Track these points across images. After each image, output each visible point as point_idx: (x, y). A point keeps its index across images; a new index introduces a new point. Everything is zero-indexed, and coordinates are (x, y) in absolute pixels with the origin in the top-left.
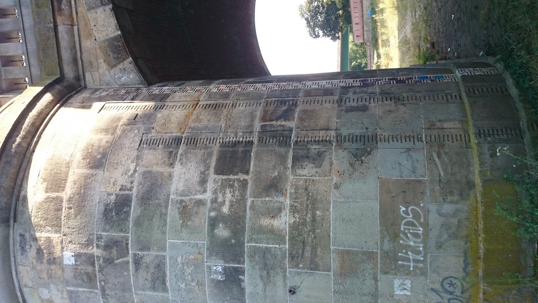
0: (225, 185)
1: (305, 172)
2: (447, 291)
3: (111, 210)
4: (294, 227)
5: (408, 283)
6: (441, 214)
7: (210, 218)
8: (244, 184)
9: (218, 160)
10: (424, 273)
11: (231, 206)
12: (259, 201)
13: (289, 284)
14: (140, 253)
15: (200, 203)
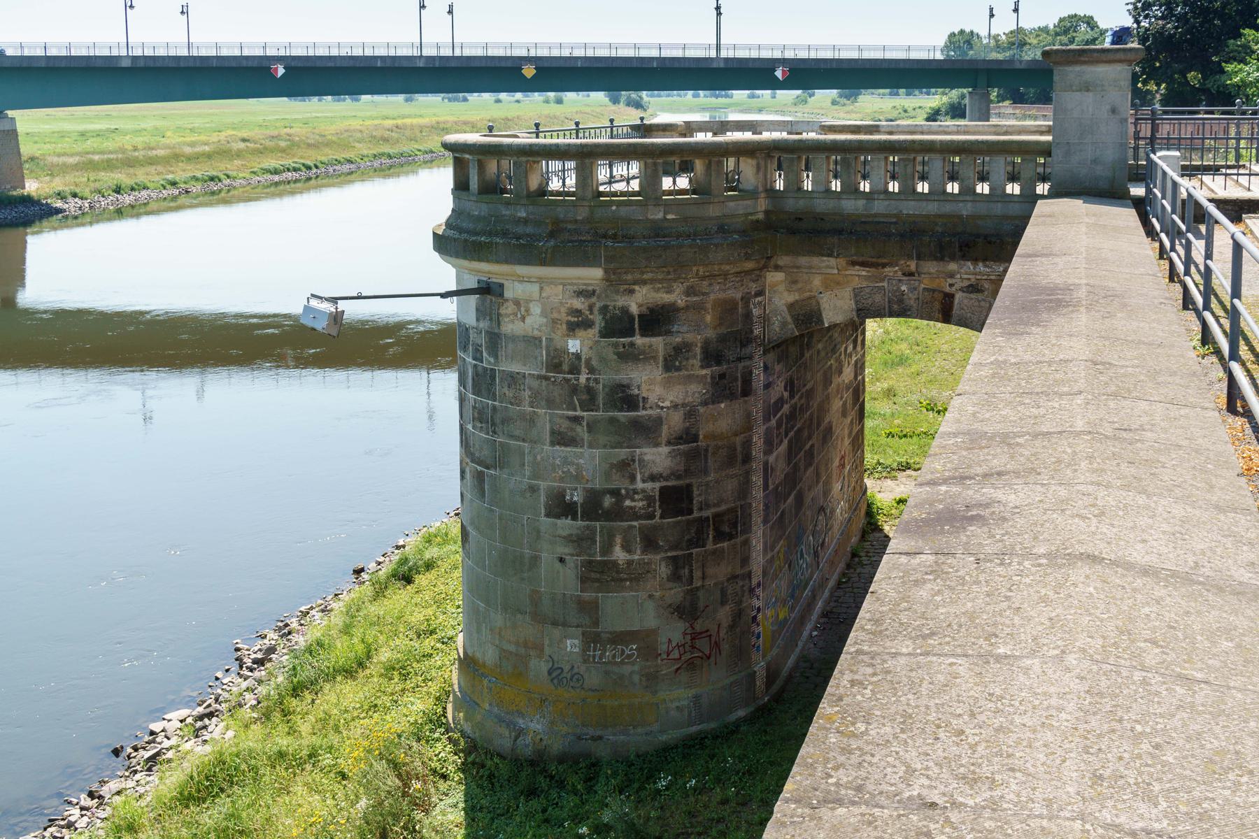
0: (649, 499)
1: (663, 569)
2: (572, 677)
3: (623, 392)
4: (615, 563)
5: (577, 650)
6: (632, 673)
7: (619, 490)
9: (674, 487)
10: (585, 661)
11: (631, 508)
14: (585, 424)
15: (633, 479)
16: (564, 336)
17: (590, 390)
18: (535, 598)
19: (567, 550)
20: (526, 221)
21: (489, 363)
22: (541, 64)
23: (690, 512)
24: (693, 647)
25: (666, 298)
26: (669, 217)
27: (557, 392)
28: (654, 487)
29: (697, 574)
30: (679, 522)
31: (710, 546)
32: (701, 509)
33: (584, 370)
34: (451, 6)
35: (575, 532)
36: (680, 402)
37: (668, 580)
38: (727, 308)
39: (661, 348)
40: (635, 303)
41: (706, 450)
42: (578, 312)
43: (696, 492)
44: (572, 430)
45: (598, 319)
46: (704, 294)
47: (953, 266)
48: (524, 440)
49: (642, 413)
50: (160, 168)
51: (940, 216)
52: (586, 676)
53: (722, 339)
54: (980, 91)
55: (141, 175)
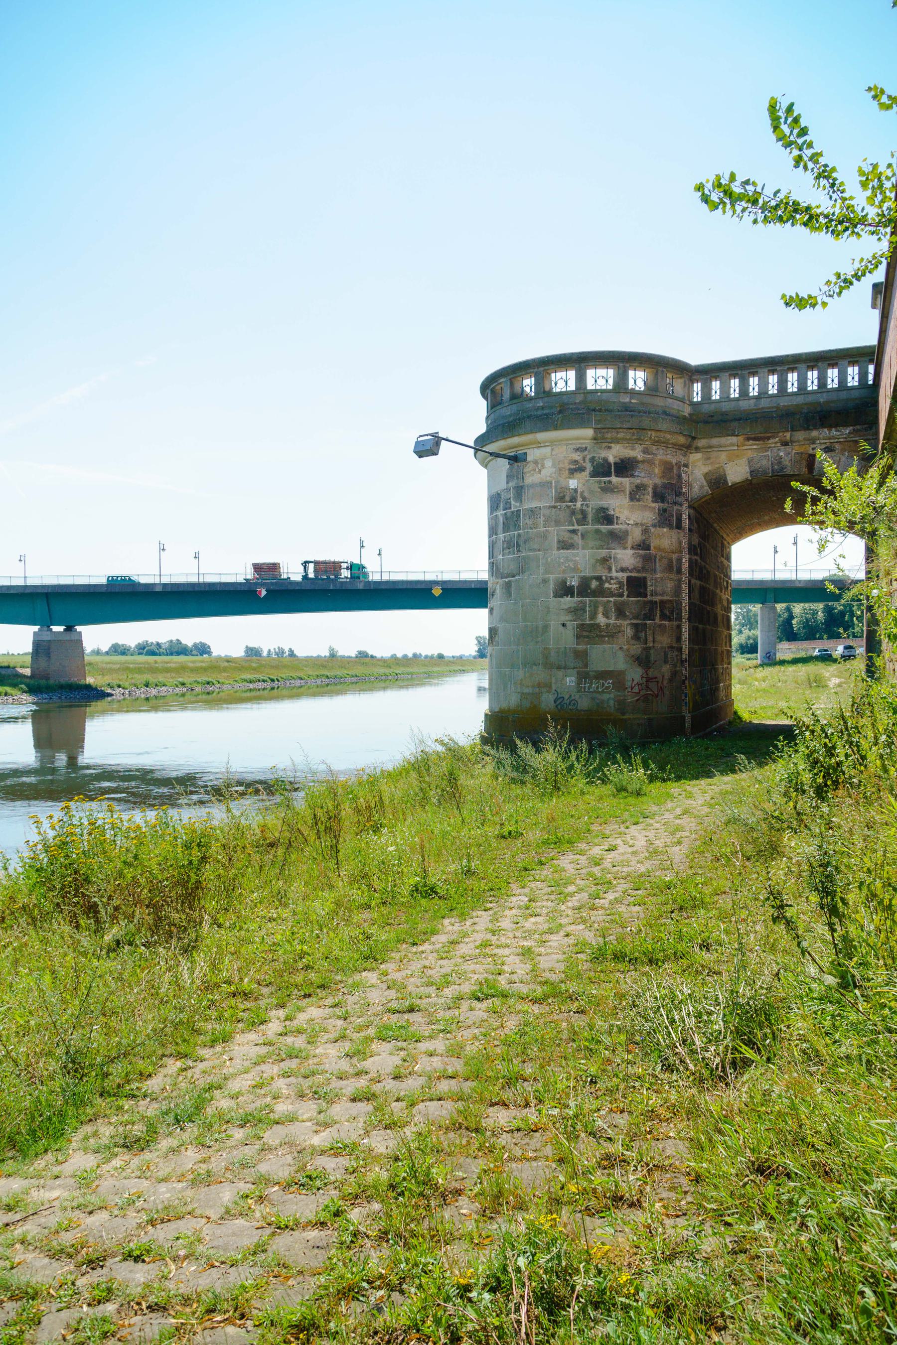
0: (620, 583)
1: (629, 630)
4: (598, 625)
5: (573, 684)
6: (608, 700)
8: (621, 595)
9: (635, 577)
10: (578, 692)
11: (609, 589)
12: (612, 605)
13: (568, 623)
15: (610, 569)
16: (567, 478)
17: (583, 513)
18: (546, 655)
19: (567, 618)
20: (543, 408)
21: (516, 507)
22: (445, 586)
23: (646, 597)
24: (648, 687)
25: (630, 453)
26: (633, 401)
27: (563, 515)
28: (623, 576)
29: (650, 638)
30: (638, 601)
31: (657, 621)
32: (652, 595)
33: (579, 499)
34: (380, 550)
35: (573, 606)
36: (639, 522)
37: (632, 638)
38: (668, 468)
39: (628, 486)
40: (613, 454)
41: (655, 557)
42: (576, 462)
43: (649, 584)
44: (572, 538)
45: (589, 467)
46: (654, 454)
47: (815, 433)
48: (539, 550)
49: (616, 526)
50: (173, 675)
51: (805, 404)
52: (579, 701)
53: (665, 486)
54: (768, 605)
55: (161, 678)
